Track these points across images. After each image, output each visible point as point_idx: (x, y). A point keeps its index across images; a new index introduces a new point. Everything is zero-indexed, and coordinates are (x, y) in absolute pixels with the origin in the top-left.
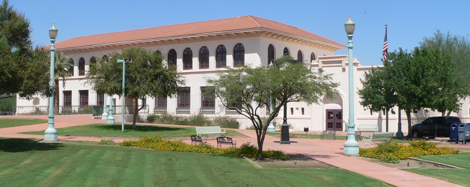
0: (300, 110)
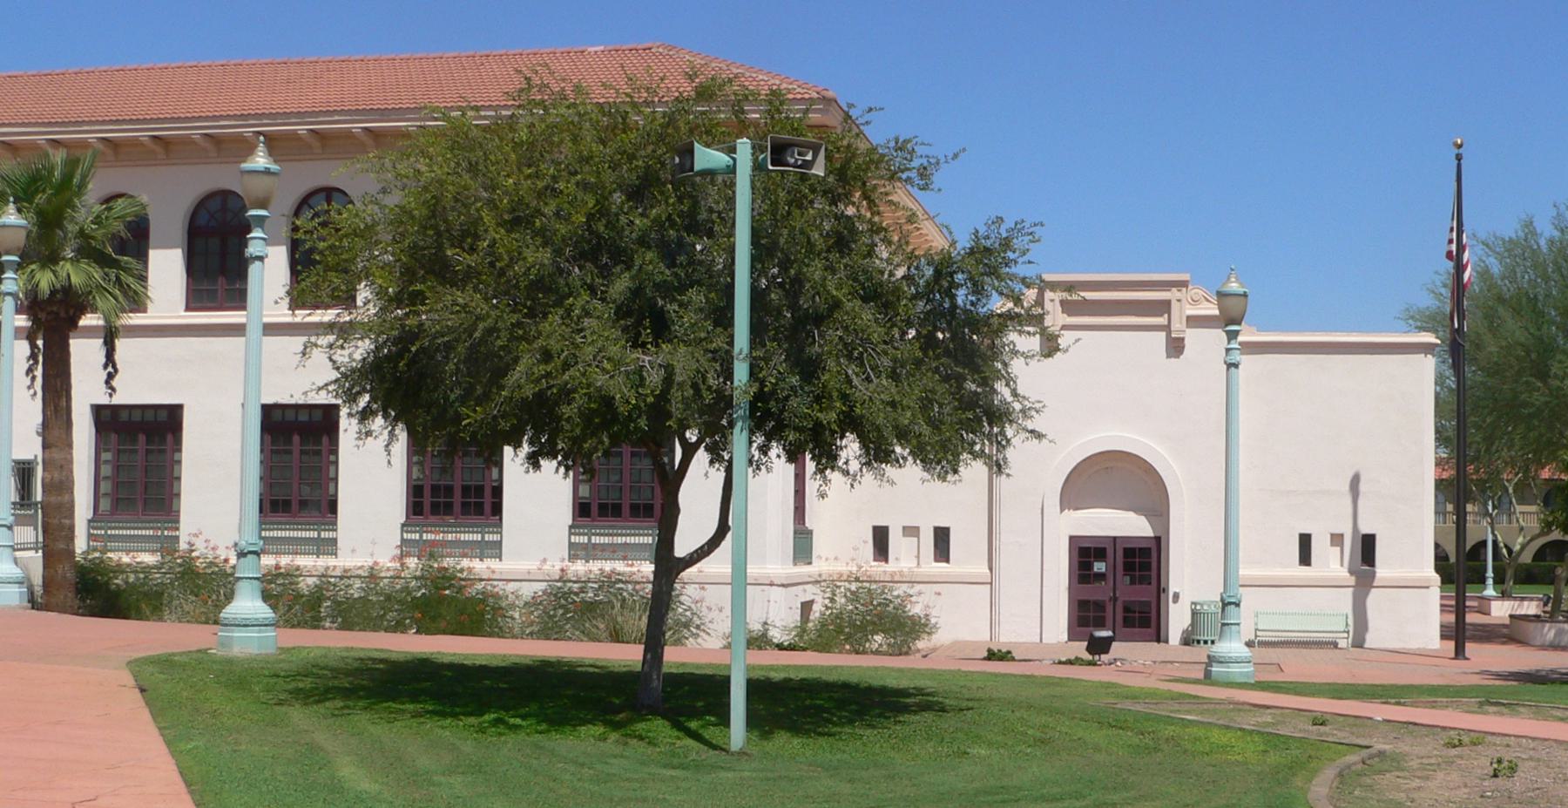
0: (928, 539)
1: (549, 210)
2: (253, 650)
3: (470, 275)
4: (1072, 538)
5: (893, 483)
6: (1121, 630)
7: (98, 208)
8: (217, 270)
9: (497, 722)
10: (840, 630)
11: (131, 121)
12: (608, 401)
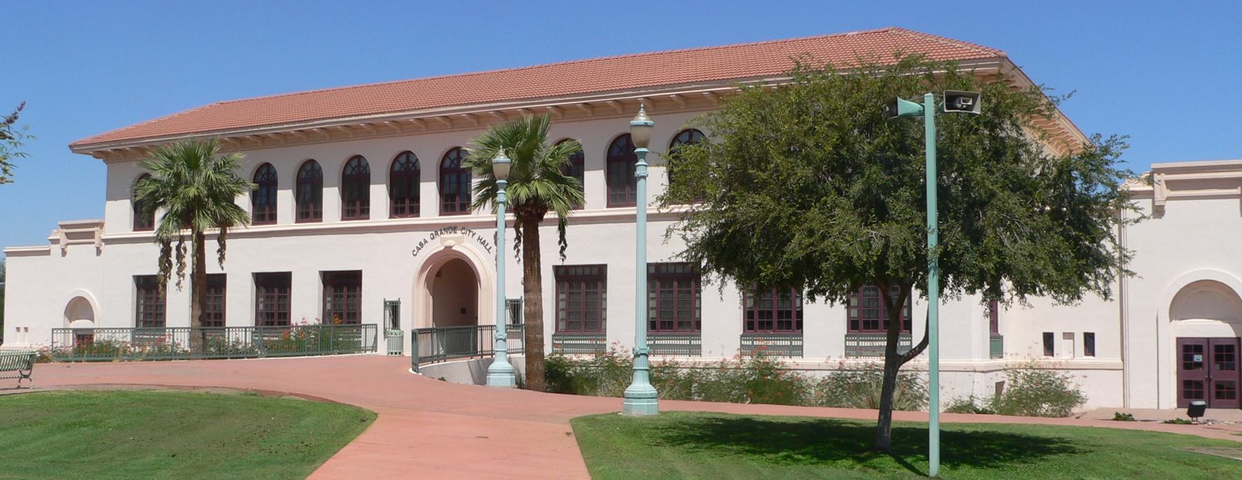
0: (1080, 341)
1: (811, 143)
2: (645, 413)
3: (765, 184)
4: (1178, 339)
5: (1031, 307)
6: (1214, 400)
7: (552, 148)
8: (622, 185)
9: (786, 457)
10: (1020, 401)
11: (571, 95)
12: (849, 259)
